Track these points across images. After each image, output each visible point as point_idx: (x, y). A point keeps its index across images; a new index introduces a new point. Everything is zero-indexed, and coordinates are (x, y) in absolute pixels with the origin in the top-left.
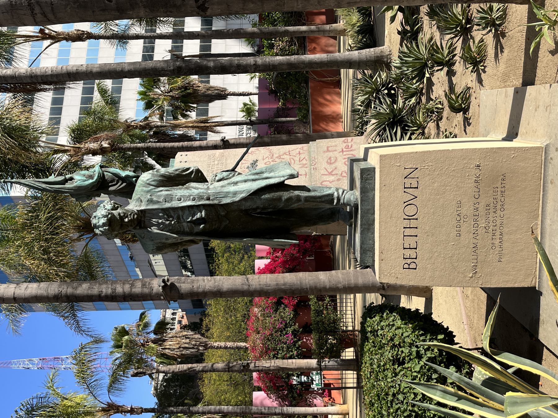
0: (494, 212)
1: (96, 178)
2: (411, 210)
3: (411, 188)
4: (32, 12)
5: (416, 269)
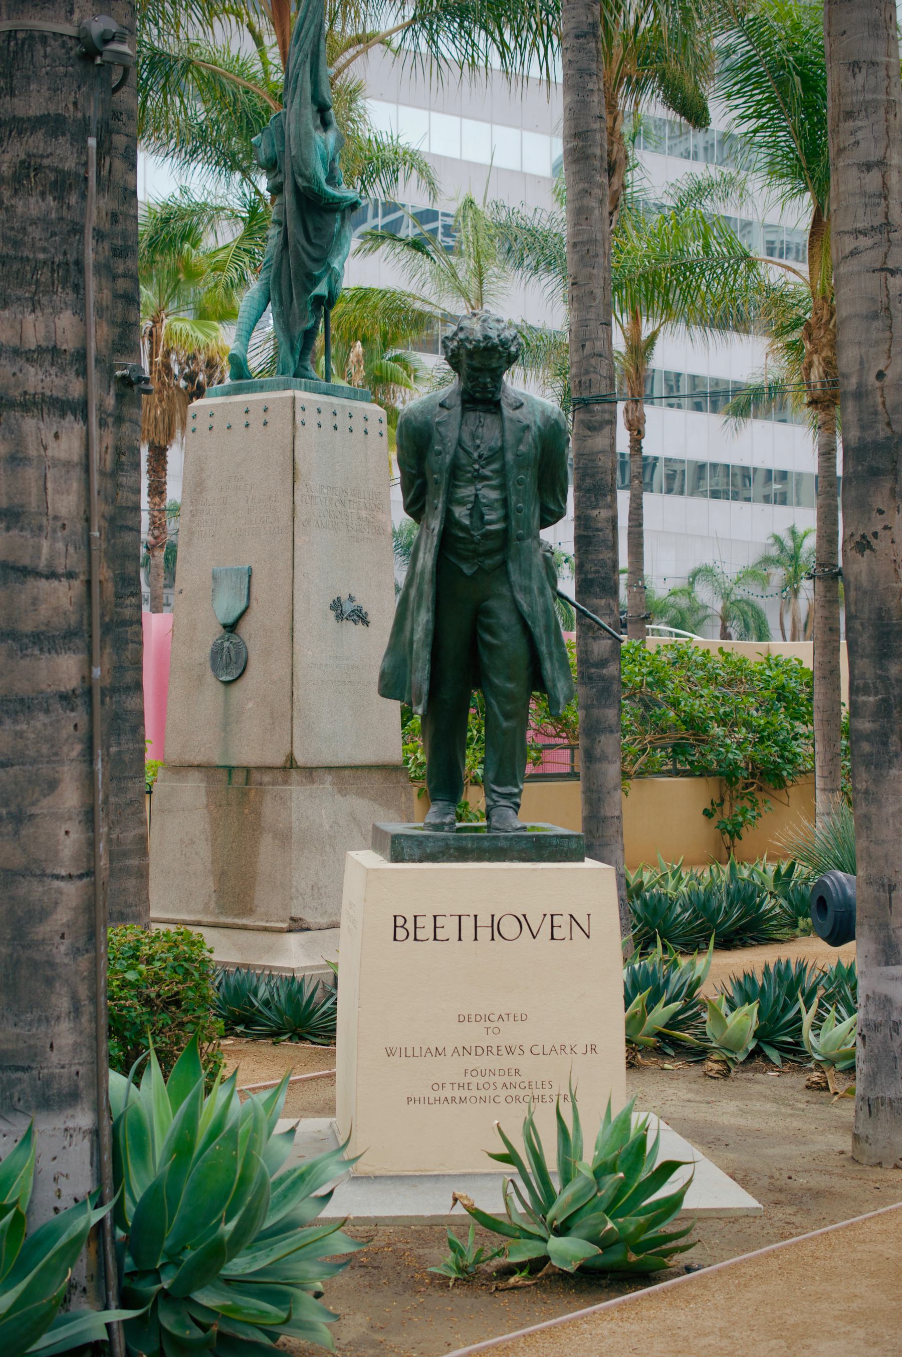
0: (505, 1085)
1: (329, 189)
2: (509, 927)
3: (552, 927)
4: (860, 232)
5: (395, 939)
